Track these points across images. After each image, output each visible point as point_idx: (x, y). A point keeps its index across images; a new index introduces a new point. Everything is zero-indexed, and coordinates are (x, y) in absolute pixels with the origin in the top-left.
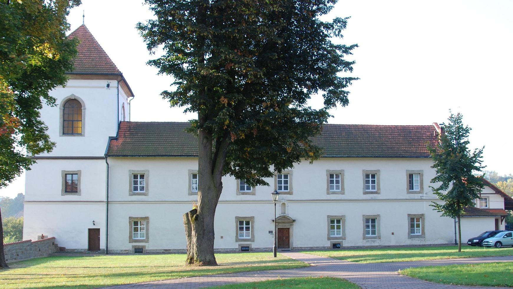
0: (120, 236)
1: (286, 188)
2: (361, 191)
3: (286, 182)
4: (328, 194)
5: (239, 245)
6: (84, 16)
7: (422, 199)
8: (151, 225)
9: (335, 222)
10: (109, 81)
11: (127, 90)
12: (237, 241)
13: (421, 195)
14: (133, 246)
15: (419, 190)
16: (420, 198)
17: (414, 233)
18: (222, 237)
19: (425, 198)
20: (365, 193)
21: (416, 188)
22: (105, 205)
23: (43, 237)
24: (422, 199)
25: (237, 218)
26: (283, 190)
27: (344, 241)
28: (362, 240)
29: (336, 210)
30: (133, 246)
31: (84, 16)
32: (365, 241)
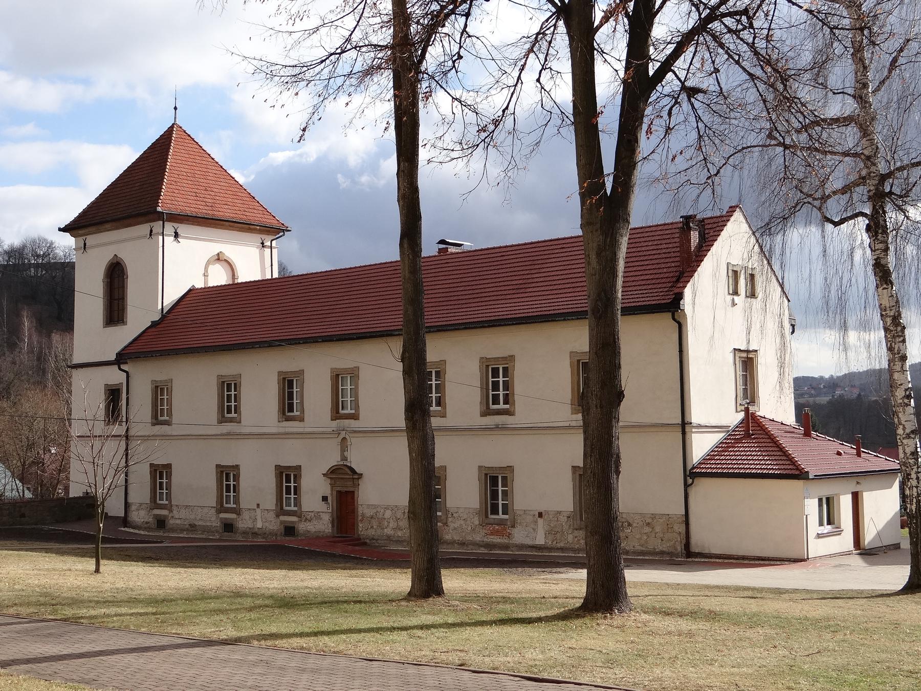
2: (477, 408)
3: (507, 386)
6: (175, 108)
9: (228, 476)
10: (152, 224)
20: (486, 412)
31: (175, 108)
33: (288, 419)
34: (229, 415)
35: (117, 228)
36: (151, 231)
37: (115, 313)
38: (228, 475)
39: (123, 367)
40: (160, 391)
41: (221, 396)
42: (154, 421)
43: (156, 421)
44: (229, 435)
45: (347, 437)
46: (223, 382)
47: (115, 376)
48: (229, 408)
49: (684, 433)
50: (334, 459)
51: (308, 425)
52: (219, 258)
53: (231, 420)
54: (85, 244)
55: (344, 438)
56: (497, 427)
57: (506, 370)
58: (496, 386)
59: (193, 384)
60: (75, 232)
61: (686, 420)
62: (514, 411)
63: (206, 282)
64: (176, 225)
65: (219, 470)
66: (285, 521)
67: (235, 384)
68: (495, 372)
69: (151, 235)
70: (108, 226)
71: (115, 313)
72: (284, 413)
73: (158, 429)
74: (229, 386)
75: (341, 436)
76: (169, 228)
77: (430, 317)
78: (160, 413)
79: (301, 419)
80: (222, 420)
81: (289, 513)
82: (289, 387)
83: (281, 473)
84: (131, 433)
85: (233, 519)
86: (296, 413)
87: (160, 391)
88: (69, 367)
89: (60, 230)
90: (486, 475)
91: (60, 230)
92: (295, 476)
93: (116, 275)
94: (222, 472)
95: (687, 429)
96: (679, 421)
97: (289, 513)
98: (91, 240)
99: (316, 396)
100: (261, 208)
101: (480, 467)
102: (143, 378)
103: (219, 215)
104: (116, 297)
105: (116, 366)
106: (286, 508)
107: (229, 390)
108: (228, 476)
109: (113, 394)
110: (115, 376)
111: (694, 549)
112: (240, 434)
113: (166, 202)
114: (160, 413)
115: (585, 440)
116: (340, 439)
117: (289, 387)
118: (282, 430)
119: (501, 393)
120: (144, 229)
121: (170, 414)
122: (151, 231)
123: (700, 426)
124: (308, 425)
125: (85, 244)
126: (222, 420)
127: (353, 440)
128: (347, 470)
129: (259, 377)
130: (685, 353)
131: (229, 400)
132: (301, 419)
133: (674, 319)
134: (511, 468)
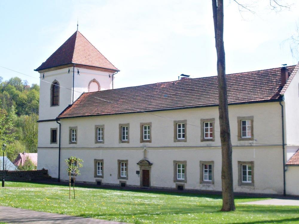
0: (161, 175)
1: (184, 136)
2: (199, 139)
3: (184, 131)
4: (175, 141)
5: (120, 182)
6: (78, 25)
7: (251, 146)
8: (105, 165)
9: (99, 163)
10: (69, 68)
11: (97, 68)
12: (118, 179)
13: (251, 142)
14: (96, 180)
15: (250, 137)
16: (250, 145)
17: (246, 180)
18: (111, 175)
19: (254, 145)
20: (203, 140)
21: (248, 136)
22: (58, 150)
23: (44, 169)
24: (251, 146)
25: (200, 161)
26: (182, 138)
27: (185, 184)
28: (199, 184)
29: (180, 156)
30: (96, 180)
31: (78, 25)
32: (201, 185)
33: (123, 142)
34: (73, 141)
35: (56, 69)
36: (69, 71)
37: (55, 102)
38: (123, 164)
39: (59, 122)
40: (73, 132)
41: (142, 131)
42: (70, 142)
43: (71, 142)
44: (74, 148)
45: (147, 149)
46: (97, 128)
47: (55, 125)
48: (73, 138)
49: (284, 148)
50: (141, 158)
51: (189, 143)
52: (94, 81)
53: (100, 142)
54: (44, 76)
55: (145, 150)
56: (208, 146)
57: (183, 125)
58: (180, 131)
59: (86, 129)
60: (40, 71)
61: (285, 143)
62: (214, 140)
63: (89, 91)
64: (78, 68)
65: (95, 161)
66: (178, 184)
67: (102, 129)
68: (179, 126)
69: (69, 72)
70: (52, 69)
71: (55, 102)
72: (121, 140)
73: (72, 145)
74: (99, 129)
75: (144, 149)
76: (76, 69)
77: (230, 100)
78: (73, 138)
79: (103, 142)
80: (97, 142)
81: (99, 177)
82: (99, 131)
83: (120, 163)
84: (61, 146)
85: (124, 182)
86: (126, 140)
87: (73, 132)
88: (37, 122)
89: (35, 70)
90: (203, 164)
91: (35, 70)
92: (101, 163)
93: (55, 88)
94: (96, 162)
95: (285, 147)
96: (282, 144)
97: (99, 177)
98: (47, 74)
99: (135, 133)
100: (109, 63)
101: (200, 161)
102: (66, 126)
103: (94, 65)
104: (55, 95)
105: (56, 122)
106: (121, 176)
107: (99, 131)
108: (99, 163)
109: (54, 133)
110: (55, 125)
111: (287, 193)
112: (103, 148)
113: (76, 59)
114: (73, 138)
115: (222, 151)
116: (143, 150)
117: (99, 131)
118: (120, 146)
119: (182, 133)
120: (66, 70)
121: (103, 138)
122: (69, 71)
123: (63, 148)
124: (189, 143)
125: (44, 76)
126: (97, 142)
127: (149, 150)
128: (146, 161)
129: (111, 127)
130: (284, 118)
131: (99, 135)
132: (128, 142)
133: (280, 104)
134: (213, 162)
